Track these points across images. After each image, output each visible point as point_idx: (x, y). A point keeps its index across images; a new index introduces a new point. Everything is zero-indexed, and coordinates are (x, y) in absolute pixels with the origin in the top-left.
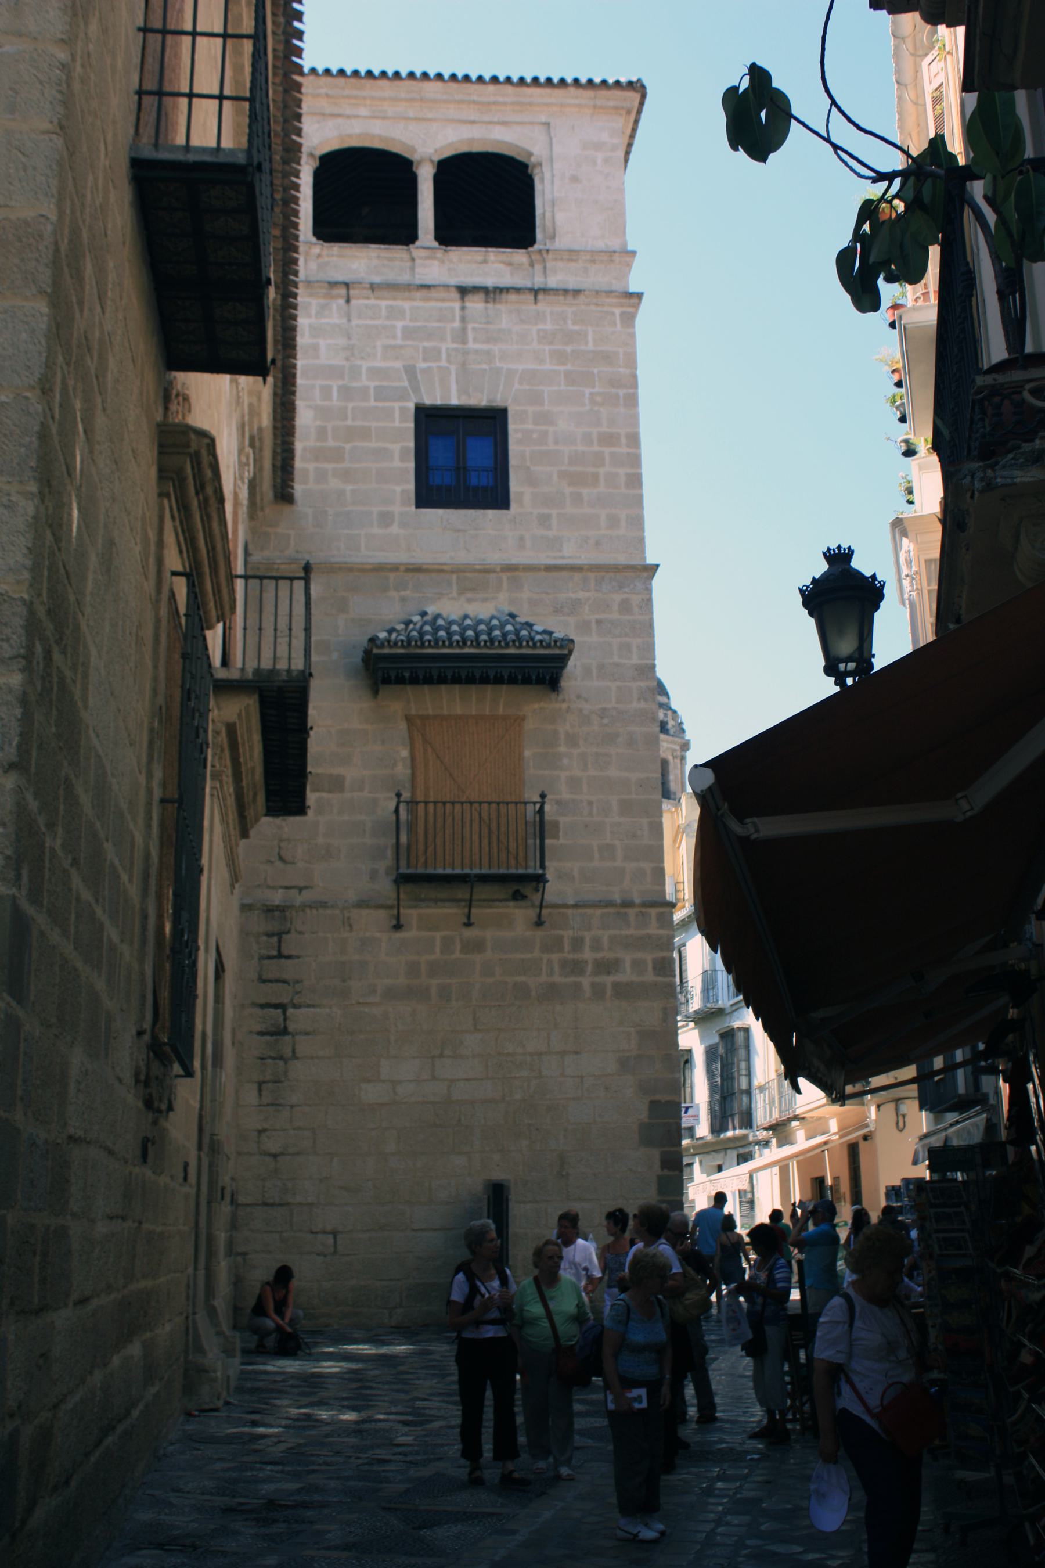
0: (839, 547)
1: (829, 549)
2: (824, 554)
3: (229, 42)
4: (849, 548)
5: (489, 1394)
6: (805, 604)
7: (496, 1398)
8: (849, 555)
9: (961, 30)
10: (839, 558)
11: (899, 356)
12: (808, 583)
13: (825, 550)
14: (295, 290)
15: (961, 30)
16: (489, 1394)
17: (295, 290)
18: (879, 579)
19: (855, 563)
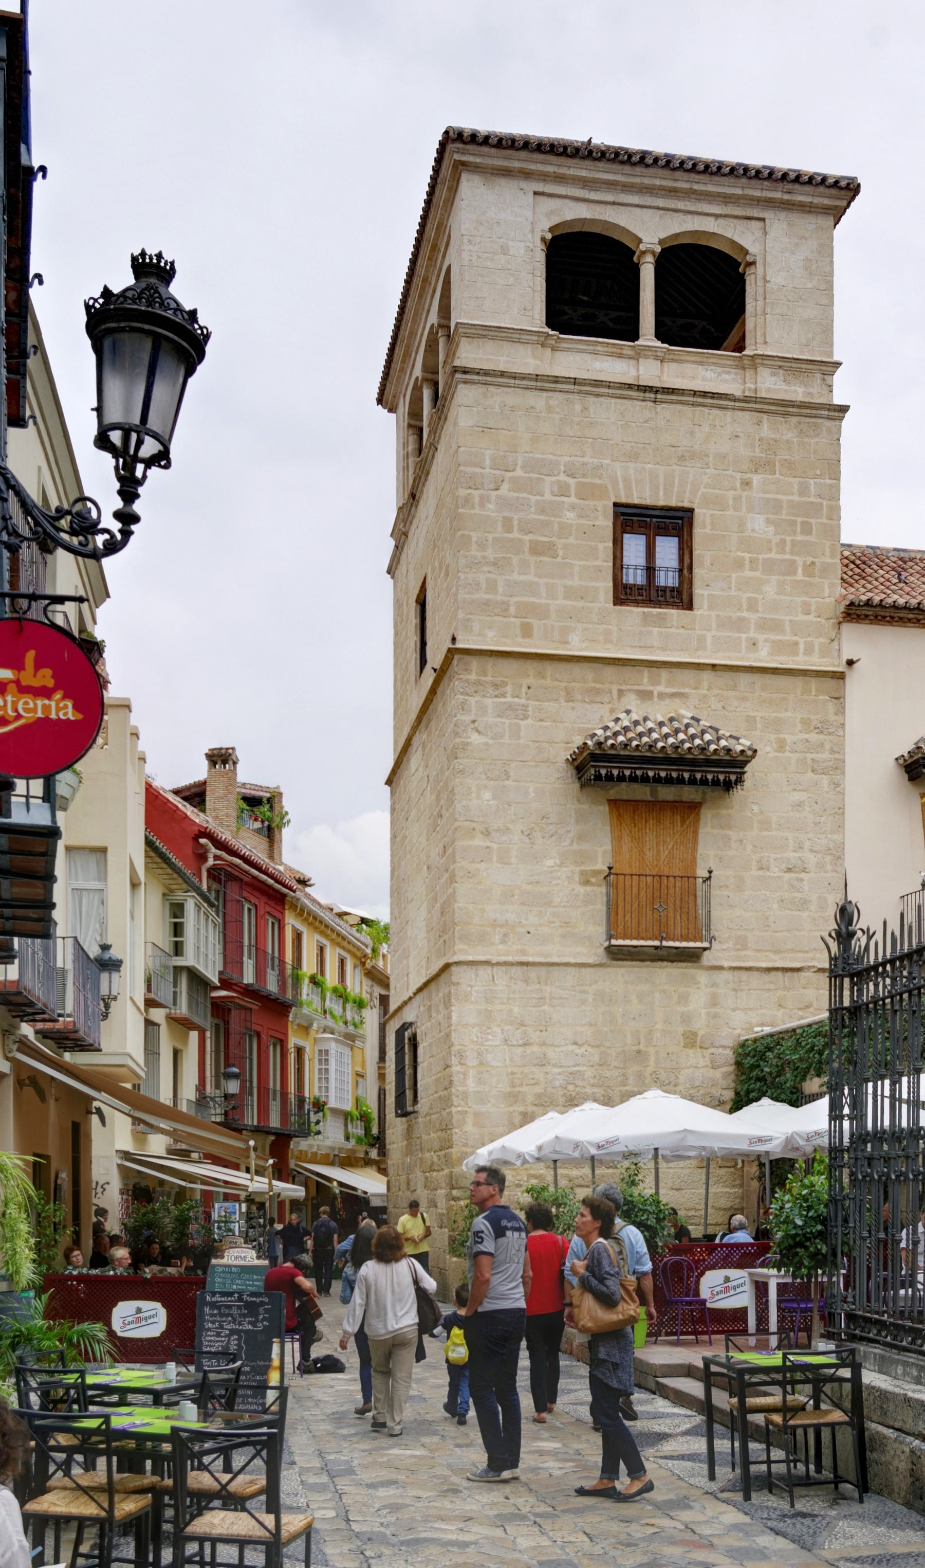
0: (159, 256)
1: (143, 254)
2: (134, 259)
3: (24, 800)
4: (172, 263)
5: (524, 1361)
6: (91, 328)
7: (534, 1370)
8: (166, 273)
9: (522, 1304)
10: (152, 271)
11: (462, 345)
12: (97, 295)
13: (137, 252)
14: (385, 1217)
15: (522, 1304)
16: (524, 1361)
17: (385, 1217)
18: (202, 323)
19: (176, 289)
